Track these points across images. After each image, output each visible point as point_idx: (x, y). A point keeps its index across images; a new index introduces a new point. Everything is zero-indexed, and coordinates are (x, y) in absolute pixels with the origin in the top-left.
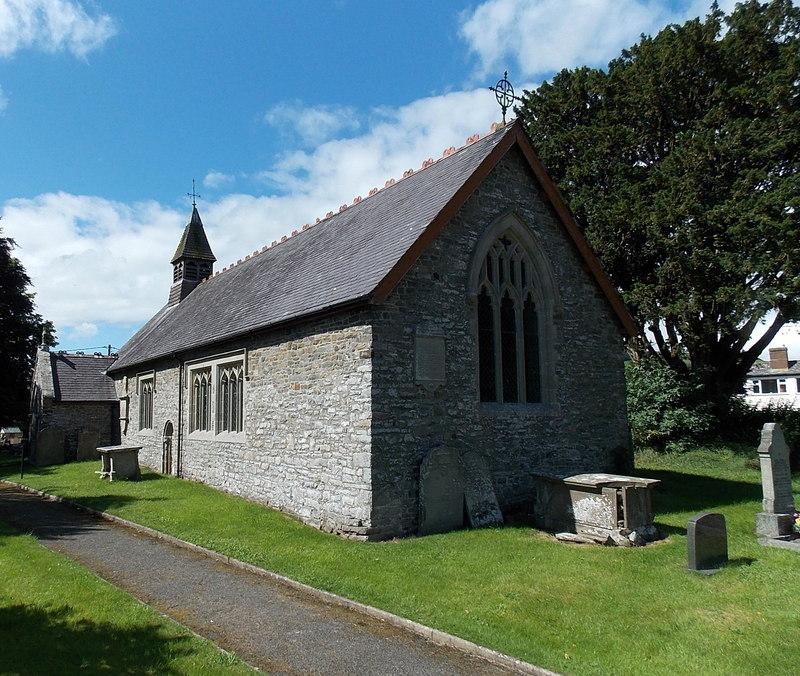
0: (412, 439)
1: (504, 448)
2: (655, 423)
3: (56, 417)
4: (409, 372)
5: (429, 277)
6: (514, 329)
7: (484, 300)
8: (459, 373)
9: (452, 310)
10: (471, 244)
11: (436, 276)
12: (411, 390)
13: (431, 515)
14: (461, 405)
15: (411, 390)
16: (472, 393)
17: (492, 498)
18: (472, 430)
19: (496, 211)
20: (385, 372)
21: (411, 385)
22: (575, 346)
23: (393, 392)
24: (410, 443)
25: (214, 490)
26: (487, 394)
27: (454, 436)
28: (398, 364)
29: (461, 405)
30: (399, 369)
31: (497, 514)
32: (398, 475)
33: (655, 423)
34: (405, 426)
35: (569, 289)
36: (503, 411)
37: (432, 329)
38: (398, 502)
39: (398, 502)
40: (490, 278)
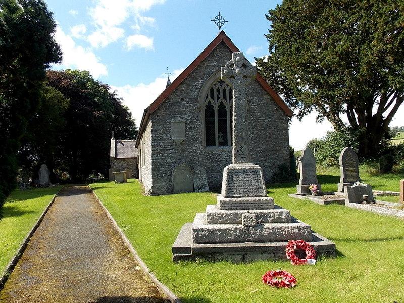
0: (170, 161)
1: (216, 164)
2: (391, 152)
3: (116, 164)
4: (169, 136)
5: (179, 100)
6: (226, 117)
7: (209, 108)
8: (193, 135)
9: (190, 112)
10: (200, 85)
11: (182, 99)
12: (170, 143)
13: (177, 188)
14: (194, 148)
15: (170, 143)
16: (200, 143)
17: (206, 182)
18: (200, 157)
19: (214, 70)
20: (158, 137)
21: (170, 141)
22: (258, 122)
23: (162, 144)
24: (169, 162)
25: (182, 193)
26: (210, 142)
27: (191, 160)
28: (164, 133)
29: (194, 148)
30: (165, 135)
31: (207, 188)
32: (164, 173)
33: (391, 152)
34: (167, 156)
35: (255, 98)
36: (210, 149)
37: (179, 119)
38: (164, 183)
39: (164, 183)
40: (212, 97)
